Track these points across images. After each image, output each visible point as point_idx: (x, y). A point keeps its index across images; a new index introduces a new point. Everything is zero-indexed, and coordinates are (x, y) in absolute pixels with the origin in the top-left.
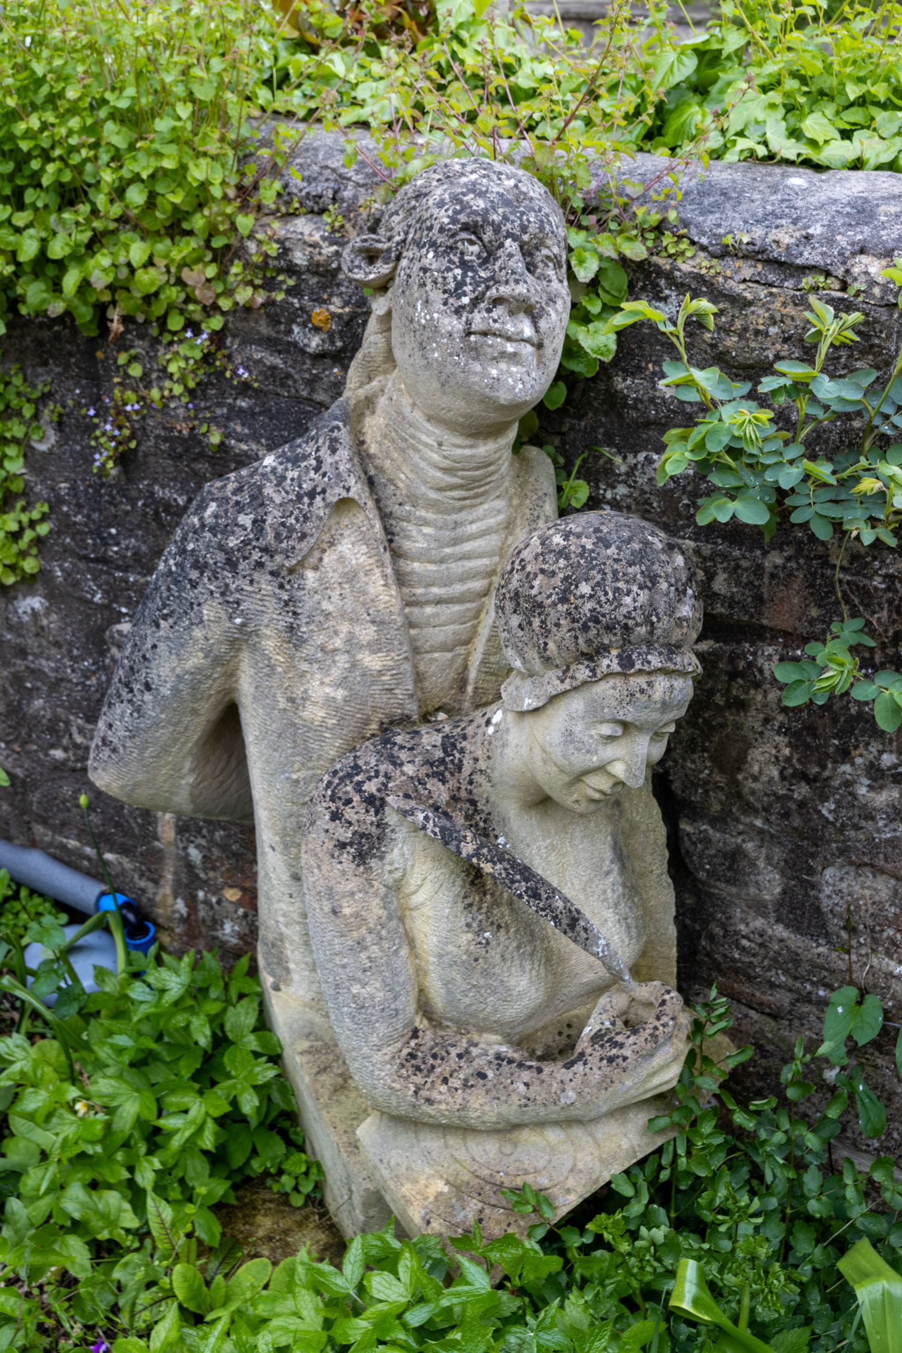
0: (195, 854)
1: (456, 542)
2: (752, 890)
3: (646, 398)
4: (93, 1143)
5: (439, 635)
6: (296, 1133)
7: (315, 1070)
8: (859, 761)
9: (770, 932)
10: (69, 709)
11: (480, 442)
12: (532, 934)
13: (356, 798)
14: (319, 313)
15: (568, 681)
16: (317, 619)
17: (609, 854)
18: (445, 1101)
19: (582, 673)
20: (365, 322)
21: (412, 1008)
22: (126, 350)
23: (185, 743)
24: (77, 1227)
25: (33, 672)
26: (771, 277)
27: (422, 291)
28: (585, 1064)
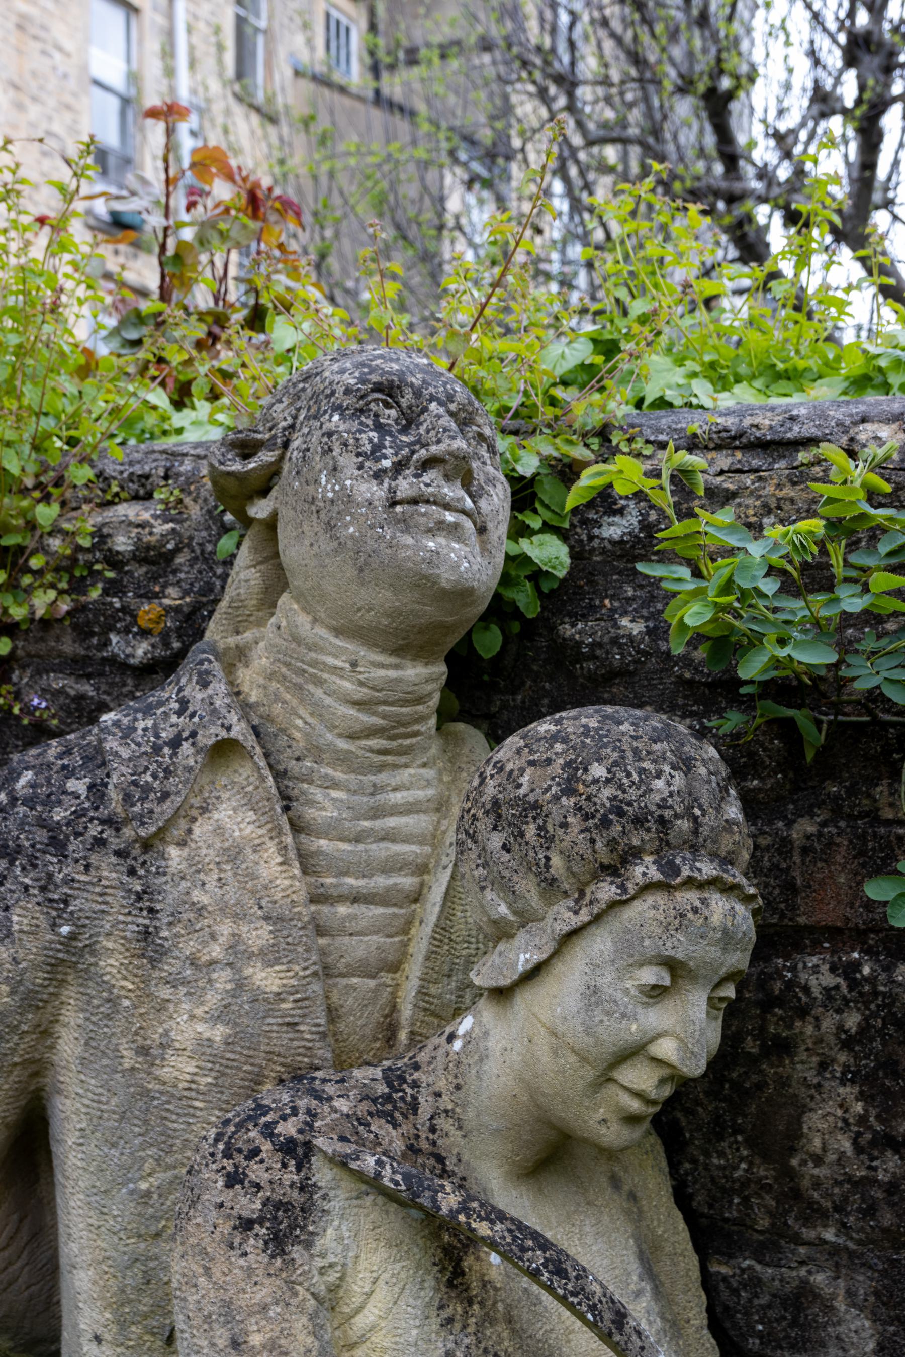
1: (377, 813)
3: (606, 639)
5: (359, 948)
11: (409, 664)
13: (267, 1147)
14: (148, 611)
17: (635, 1267)
19: (607, 891)
20: (211, 613)
26: (756, 463)
27: (328, 459)
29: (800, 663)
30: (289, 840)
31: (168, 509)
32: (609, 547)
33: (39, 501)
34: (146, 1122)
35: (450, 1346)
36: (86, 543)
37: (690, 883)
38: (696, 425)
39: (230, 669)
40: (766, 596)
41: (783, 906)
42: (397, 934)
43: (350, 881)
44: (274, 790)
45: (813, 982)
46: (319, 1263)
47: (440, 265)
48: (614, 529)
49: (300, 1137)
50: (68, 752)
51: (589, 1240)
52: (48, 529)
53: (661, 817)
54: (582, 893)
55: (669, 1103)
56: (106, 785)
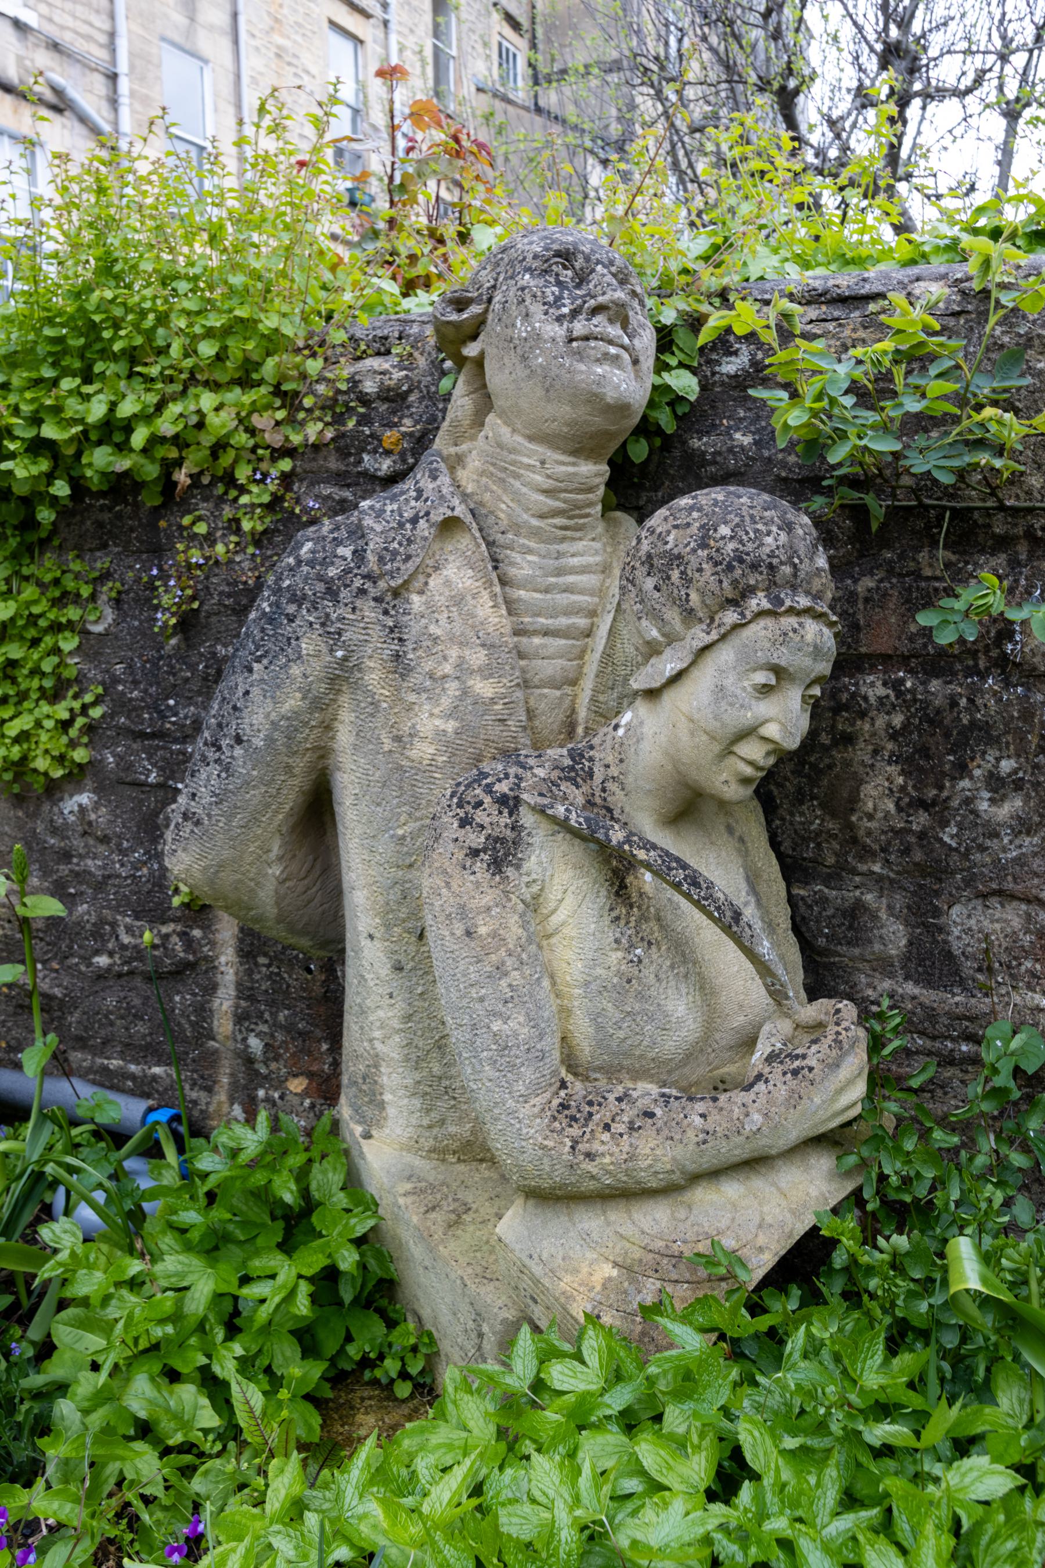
0: (255, 1044)
1: (560, 572)
2: (877, 947)
4: (162, 1321)
6: (395, 1311)
7: (422, 1209)
8: (977, 772)
10: (116, 909)
12: (683, 955)
13: (487, 800)
14: (390, 437)
17: (744, 886)
18: (610, 1154)
19: (731, 617)
21: (556, 1055)
22: (189, 512)
23: (276, 812)
24: (144, 1430)
25: (77, 874)
27: (522, 307)
28: (767, 1081)
30: (497, 589)
36: (343, 387)
37: (791, 611)
39: (452, 469)
43: (542, 620)
45: (870, 693)
46: (525, 879)
48: (730, 366)
50: (337, 528)
51: (712, 867)
54: (712, 620)
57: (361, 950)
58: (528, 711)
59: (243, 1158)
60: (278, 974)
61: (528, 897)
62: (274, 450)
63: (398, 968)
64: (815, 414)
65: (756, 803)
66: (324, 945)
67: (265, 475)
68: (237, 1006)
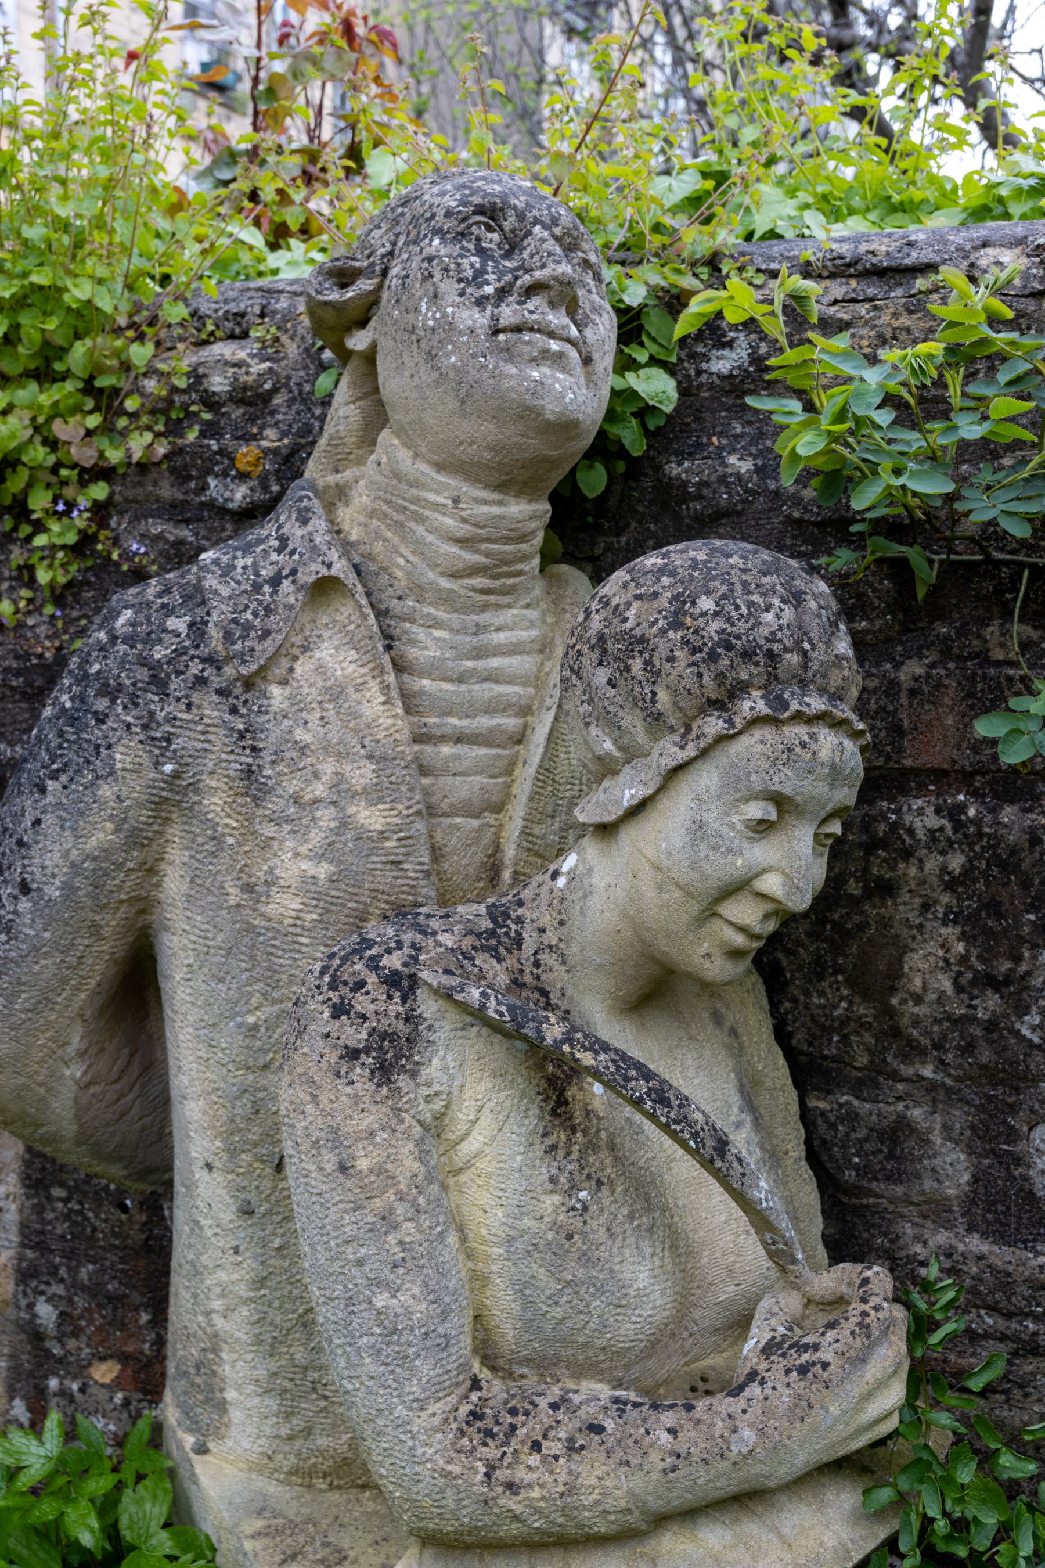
0: (46, 1313)
1: (480, 653)
2: (928, 1184)
3: (713, 478)
5: (463, 788)
7: (277, 1559)
9: (961, 1247)
11: (511, 500)
12: (647, 1199)
13: (372, 979)
14: (246, 454)
15: (690, 746)
16: (287, 755)
17: (735, 1099)
19: (713, 725)
20: (309, 454)
21: (466, 1341)
23: (77, 989)
26: (871, 291)
27: (428, 285)
28: (763, 1382)
29: (915, 494)
30: (391, 678)
31: (264, 348)
32: (717, 382)
33: (133, 341)
34: (252, 957)
35: (554, 1171)
36: (182, 383)
37: (799, 717)
38: (810, 251)
39: (330, 507)
40: (880, 427)
41: (889, 748)
42: (500, 775)
43: (453, 721)
44: (376, 629)
45: (918, 824)
46: (424, 1091)
47: (539, 123)
48: (722, 363)
49: (406, 970)
50: (167, 591)
51: (691, 1073)
52: (143, 370)
53: (770, 650)
54: (688, 728)
55: (773, 939)
56: (206, 623)
57: (195, 1184)
58: (433, 849)
59: (24, 1481)
60: (80, 1213)
61: (427, 1117)
62: (83, 470)
63: (247, 1211)
64: (835, 438)
65: (755, 978)
66: (145, 1173)
67: (71, 505)
68: (21, 1258)
